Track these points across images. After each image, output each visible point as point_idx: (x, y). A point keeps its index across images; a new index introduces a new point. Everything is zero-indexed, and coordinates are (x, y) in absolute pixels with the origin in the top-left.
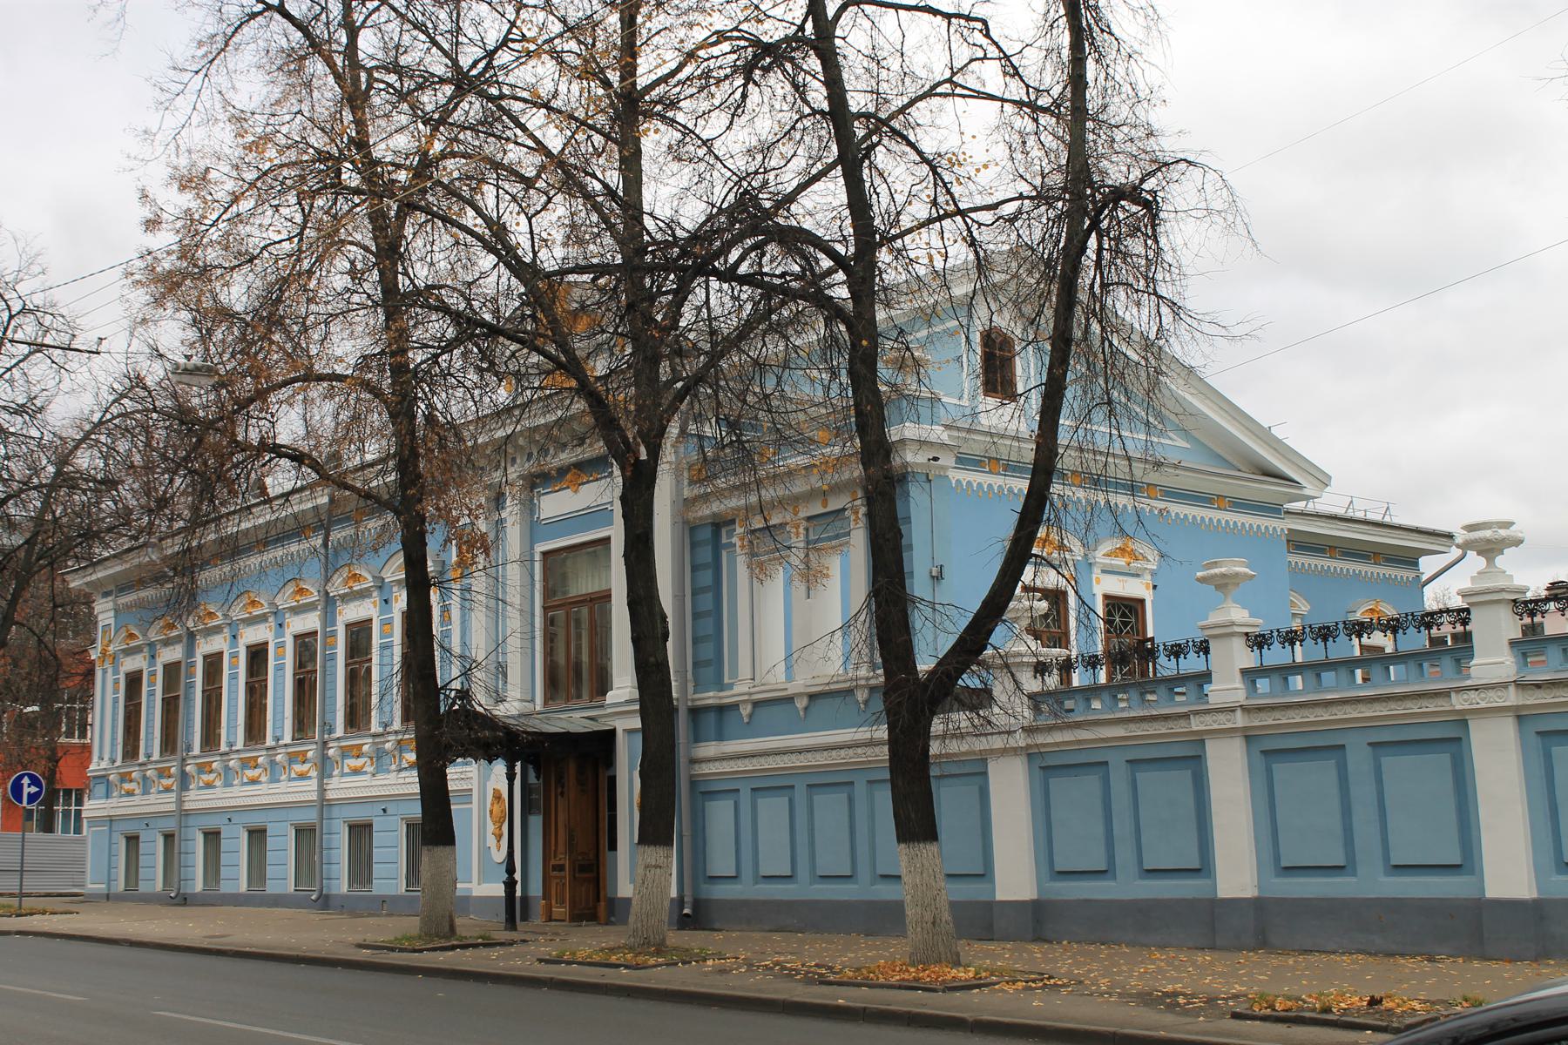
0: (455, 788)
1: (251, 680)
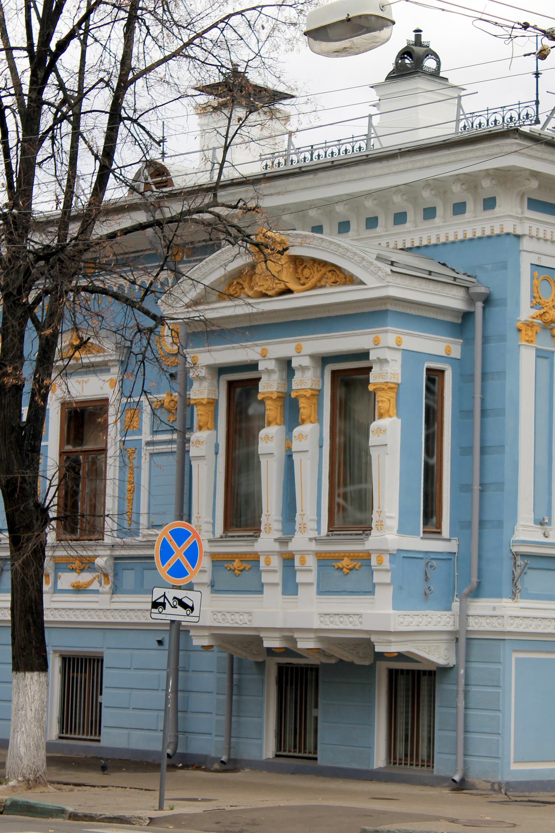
0: (52, 619)
1: (69, 448)
